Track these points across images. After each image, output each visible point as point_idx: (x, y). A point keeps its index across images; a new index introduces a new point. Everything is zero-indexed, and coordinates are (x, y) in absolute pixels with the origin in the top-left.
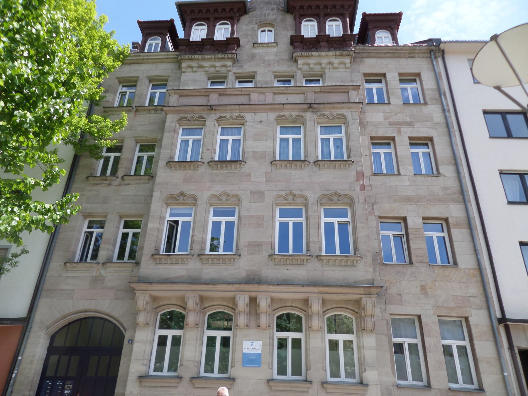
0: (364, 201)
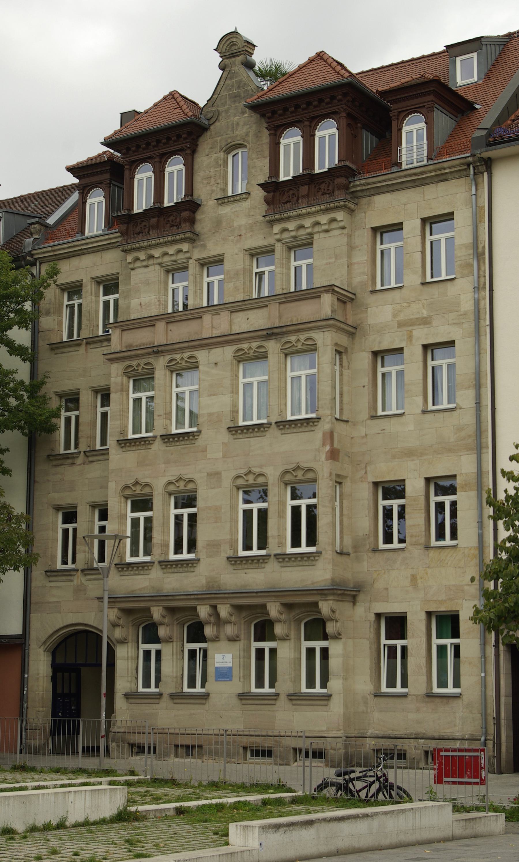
0: (328, 475)
